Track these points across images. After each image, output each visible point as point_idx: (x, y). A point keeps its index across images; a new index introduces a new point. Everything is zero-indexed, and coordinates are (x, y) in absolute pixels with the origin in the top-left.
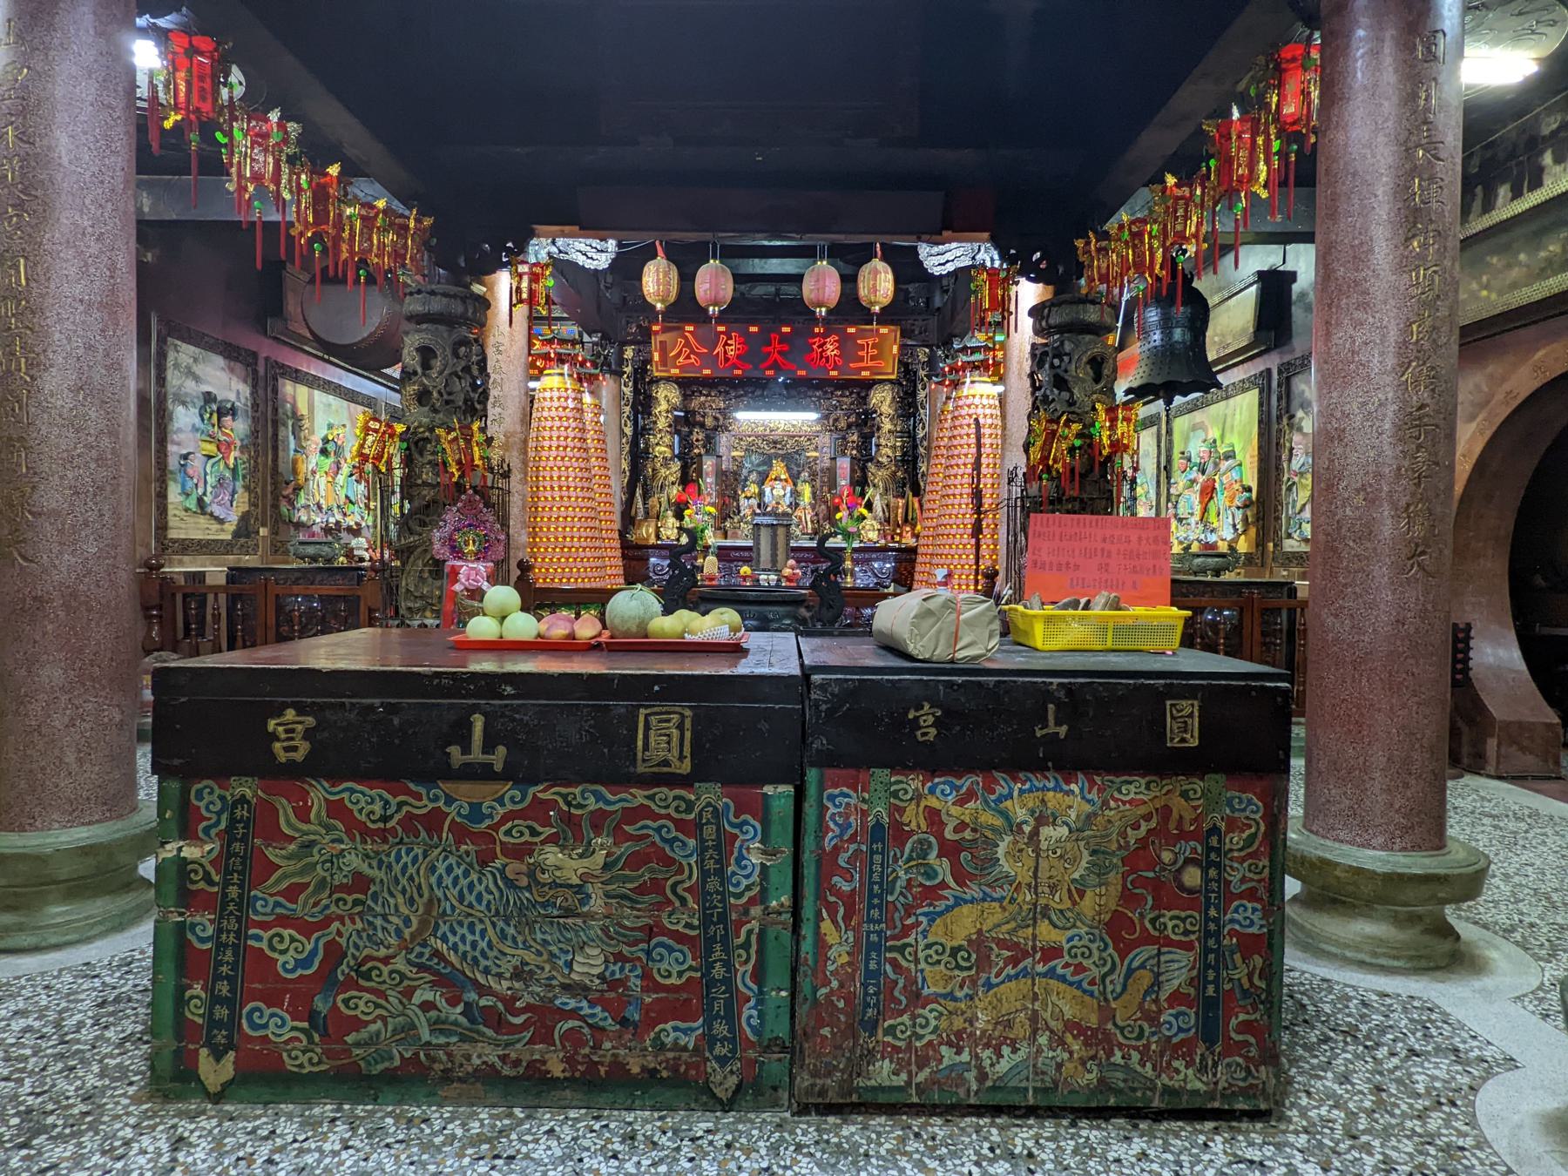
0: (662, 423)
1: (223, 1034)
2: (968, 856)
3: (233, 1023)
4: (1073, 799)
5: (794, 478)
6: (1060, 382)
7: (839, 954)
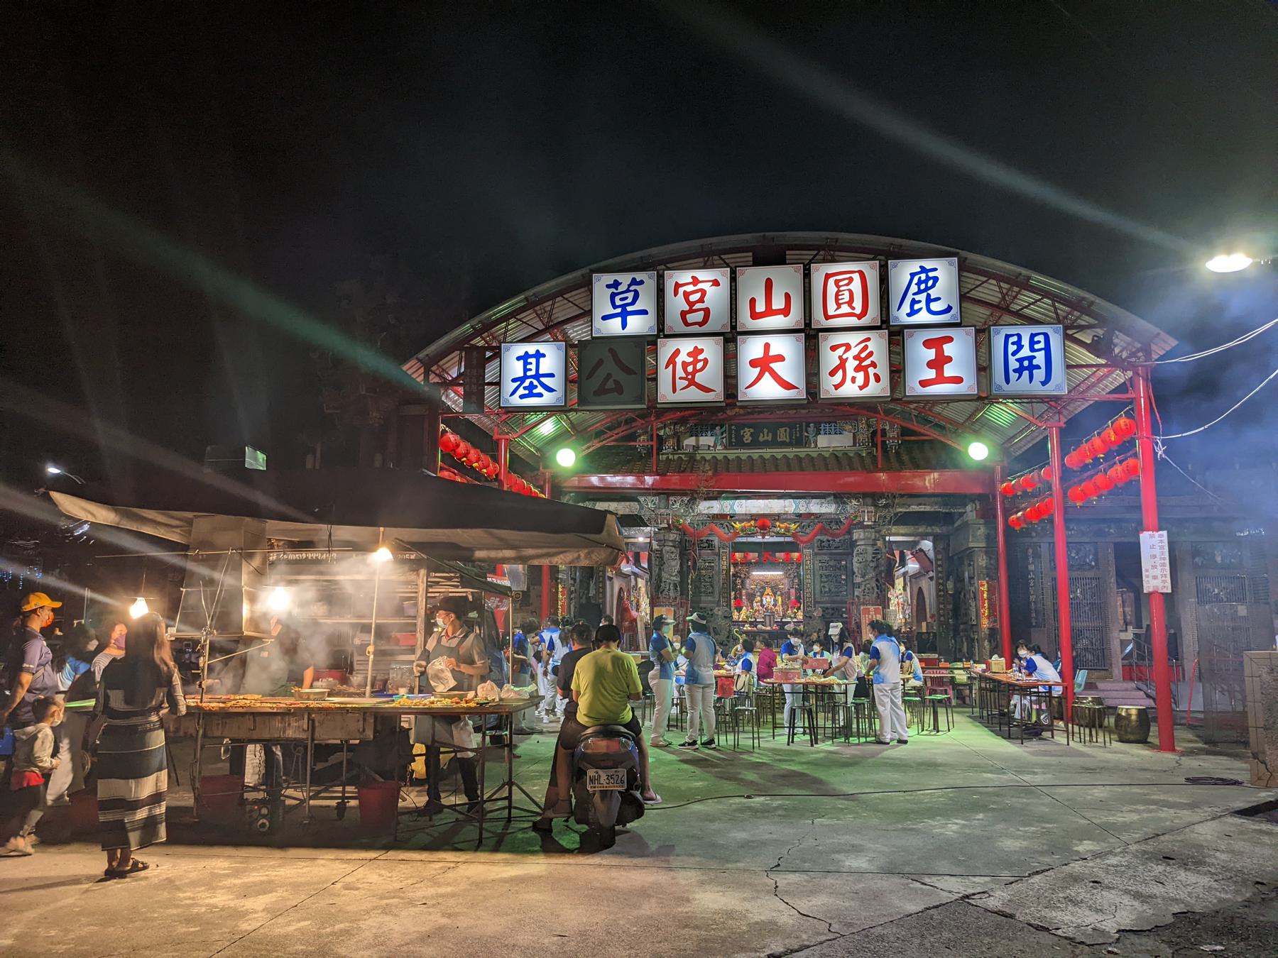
5: (775, 594)
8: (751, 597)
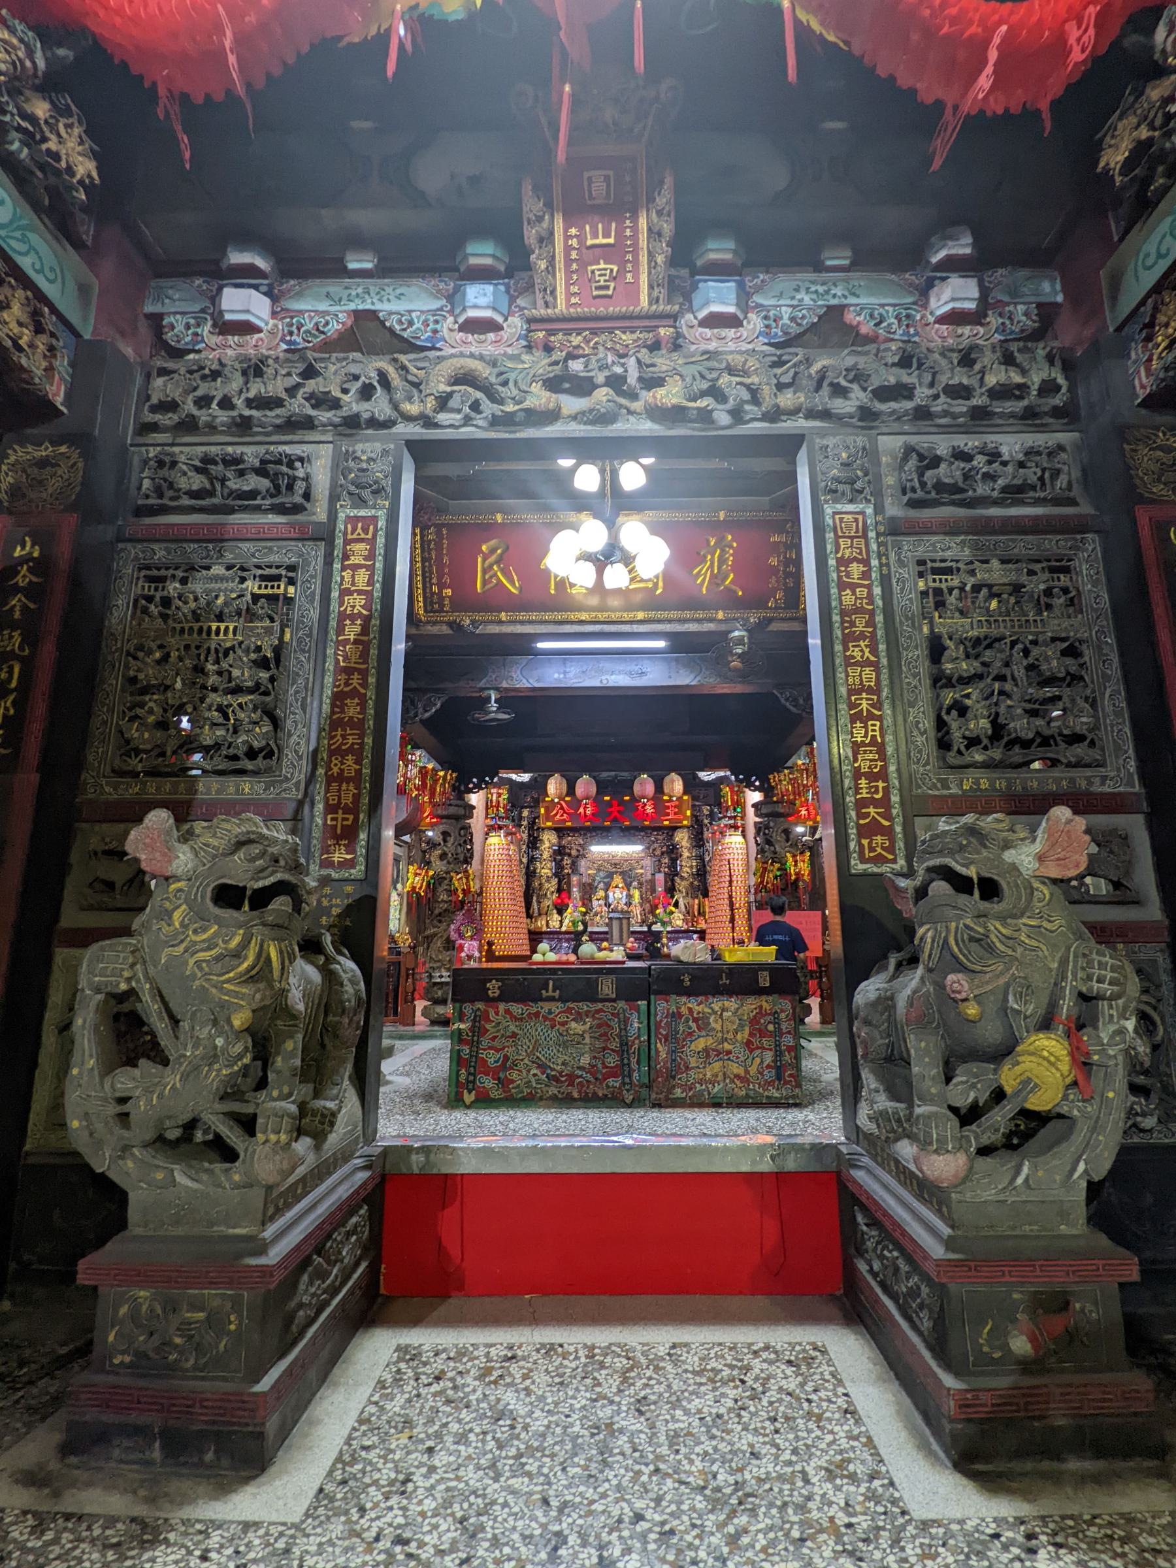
0: (546, 855)
1: (470, 1085)
2: (702, 1022)
3: (474, 1082)
4: (732, 1003)
5: (628, 886)
6: (769, 842)
7: (663, 1055)
8: (588, 891)
